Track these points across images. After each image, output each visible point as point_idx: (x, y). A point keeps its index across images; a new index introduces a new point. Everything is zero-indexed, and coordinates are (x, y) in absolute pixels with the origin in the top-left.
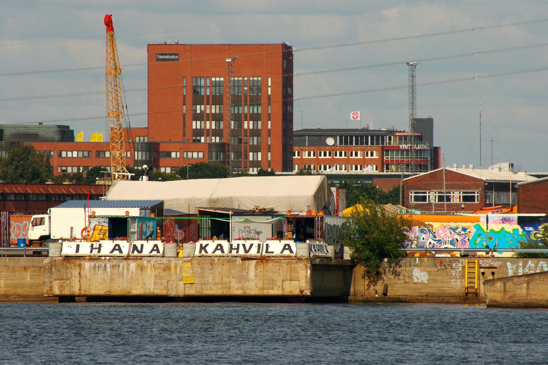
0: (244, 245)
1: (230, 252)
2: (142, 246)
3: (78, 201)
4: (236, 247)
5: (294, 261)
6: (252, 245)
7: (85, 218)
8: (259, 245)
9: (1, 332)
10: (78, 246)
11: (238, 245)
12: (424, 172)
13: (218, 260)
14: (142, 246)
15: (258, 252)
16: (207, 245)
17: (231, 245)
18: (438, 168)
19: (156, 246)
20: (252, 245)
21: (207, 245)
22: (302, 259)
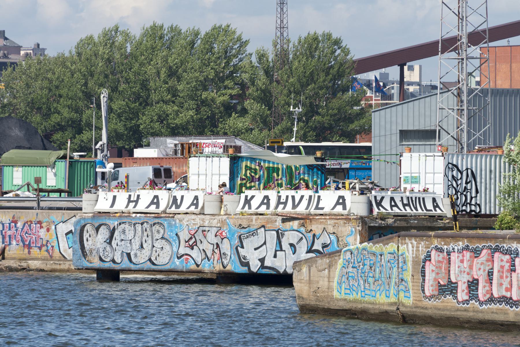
0: (293, 197)
1: (277, 207)
2: (182, 197)
3: (320, 32)
4: (284, 201)
5: (342, 222)
6: (302, 197)
7: (471, 82)
8: (310, 197)
9: (3, 325)
10: (115, 197)
11: (287, 197)
12: (70, 147)
13: (256, 220)
14: (182, 197)
15: (307, 209)
16: (253, 197)
17: (279, 197)
18: (390, 100)
19: (266, 197)
20: (302, 197)
21: (253, 197)
22: (350, 219)
